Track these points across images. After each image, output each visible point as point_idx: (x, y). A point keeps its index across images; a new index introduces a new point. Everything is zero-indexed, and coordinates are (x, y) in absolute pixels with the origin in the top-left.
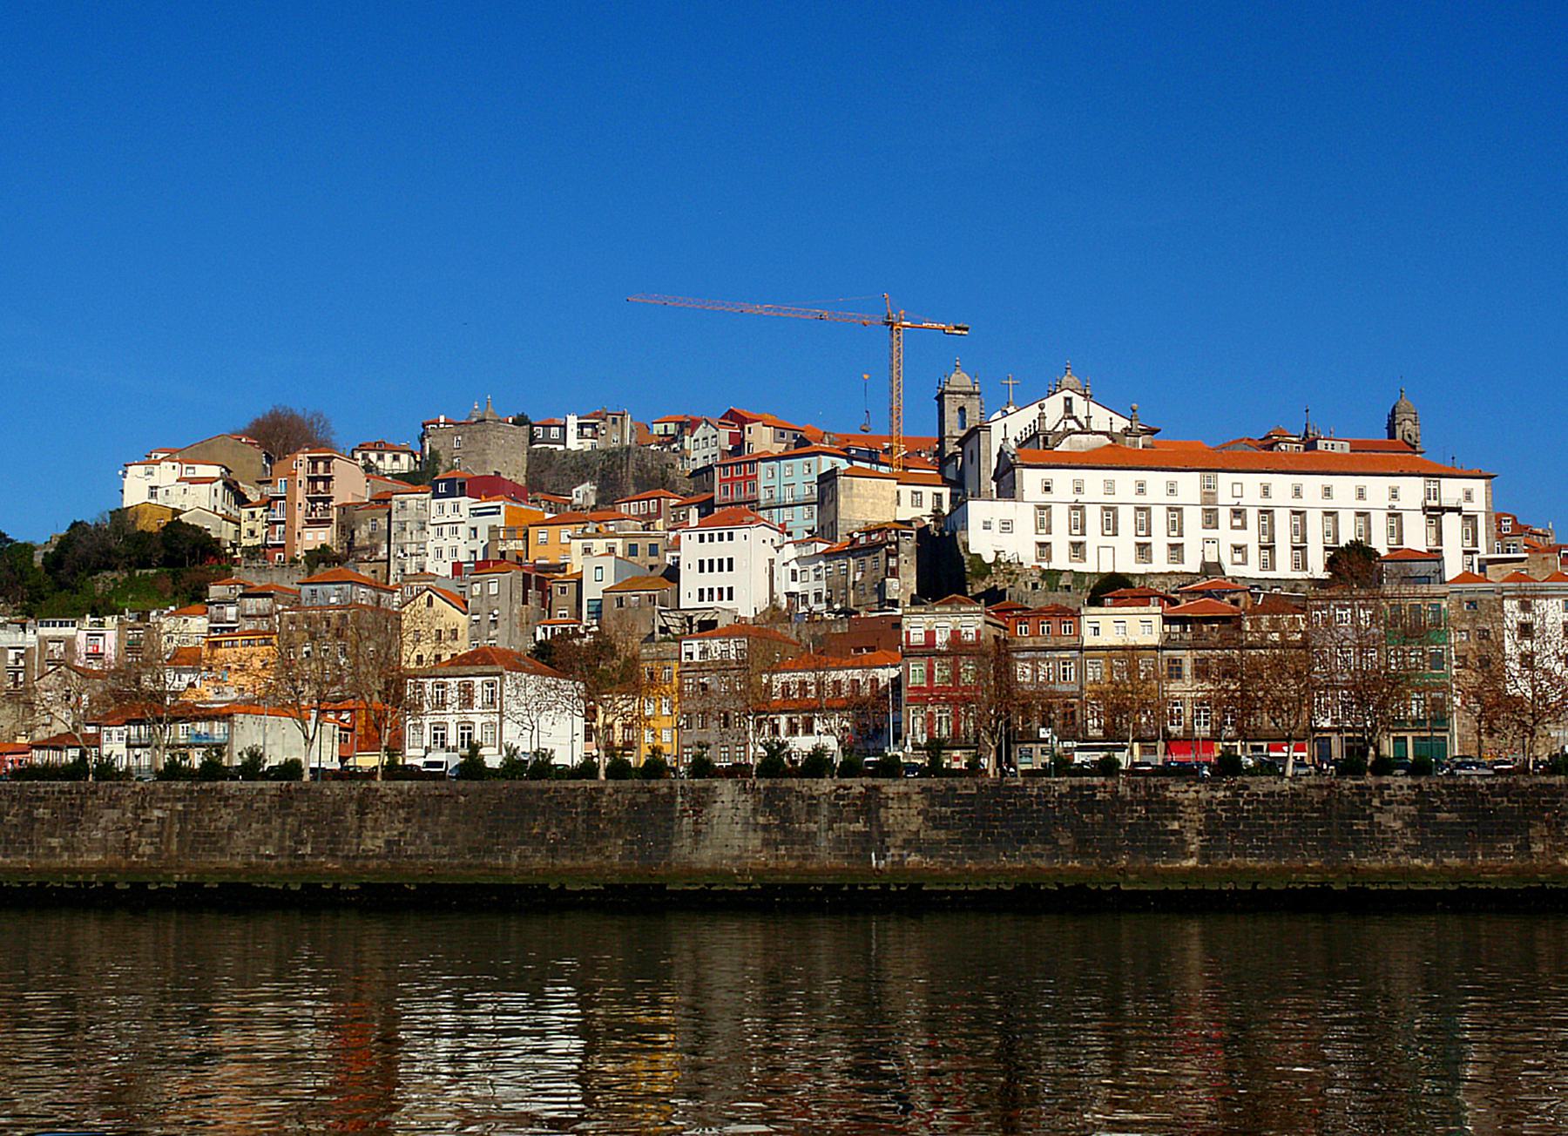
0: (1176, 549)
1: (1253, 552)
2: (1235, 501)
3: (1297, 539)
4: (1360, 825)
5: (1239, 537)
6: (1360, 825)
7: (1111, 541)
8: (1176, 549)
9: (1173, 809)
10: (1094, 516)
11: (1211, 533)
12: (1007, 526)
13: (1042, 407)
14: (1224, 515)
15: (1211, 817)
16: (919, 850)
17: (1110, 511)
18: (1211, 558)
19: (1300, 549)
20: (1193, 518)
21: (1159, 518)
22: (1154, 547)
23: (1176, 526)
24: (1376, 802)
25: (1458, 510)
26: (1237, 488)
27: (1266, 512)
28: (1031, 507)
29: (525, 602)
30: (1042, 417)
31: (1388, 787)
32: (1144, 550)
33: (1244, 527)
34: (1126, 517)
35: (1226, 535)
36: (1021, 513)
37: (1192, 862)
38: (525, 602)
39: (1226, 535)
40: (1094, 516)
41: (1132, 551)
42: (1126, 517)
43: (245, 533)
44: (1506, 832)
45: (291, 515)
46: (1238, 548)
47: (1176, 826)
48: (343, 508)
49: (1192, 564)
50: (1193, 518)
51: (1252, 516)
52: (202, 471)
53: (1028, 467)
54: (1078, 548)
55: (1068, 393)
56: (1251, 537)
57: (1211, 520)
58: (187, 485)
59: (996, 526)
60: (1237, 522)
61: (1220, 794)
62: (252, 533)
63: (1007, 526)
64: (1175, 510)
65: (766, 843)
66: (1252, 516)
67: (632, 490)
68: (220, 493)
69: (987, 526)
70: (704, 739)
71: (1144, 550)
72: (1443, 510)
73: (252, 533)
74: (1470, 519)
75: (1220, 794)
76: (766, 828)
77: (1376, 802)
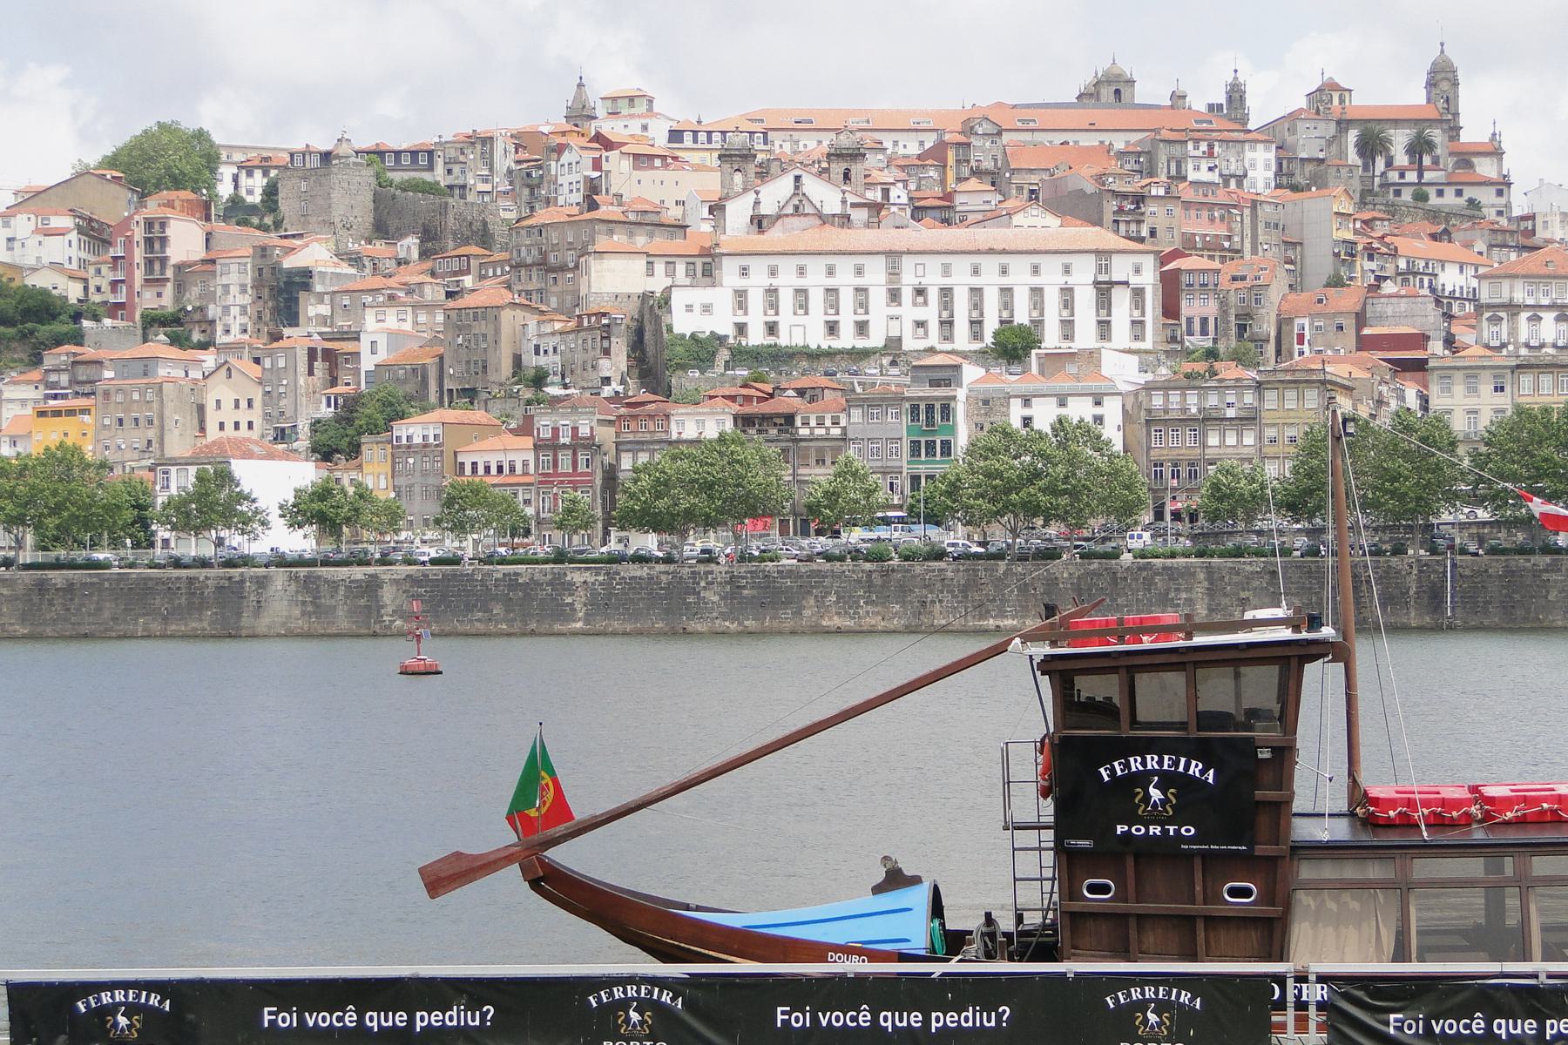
0: (862, 328)
1: (934, 327)
2: (916, 282)
3: (975, 314)
4: (691, 599)
5: (921, 314)
6: (691, 599)
7: (801, 319)
8: (862, 328)
9: (570, 588)
10: (786, 300)
11: (895, 311)
12: (707, 309)
13: (757, 193)
14: (907, 294)
15: (595, 595)
16: (401, 617)
17: (802, 293)
18: (895, 333)
19: (976, 325)
20: (878, 297)
21: (847, 299)
22: (841, 325)
23: (863, 303)
24: (703, 584)
25: (1126, 283)
26: (920, 272)
27: (946, 292)
28: (730, 292)
29: (311, 372)
30: (757, 203)
31: (711, 572)
32: (832, 328)
33: (926, 303)
34: (817, 299)
35: (909, 311)
36: (721, 297)
37: (579, 625)
38: (311, 372)
39: (909, 311)
40: (786, 300)
41: (822, 329)
42: (817, 299)
43: (92, 289)
44: (786, 604)
45: (130, 274)
46: (920, 324)
47: (569, 600)
48: (179, 268)
49: (876, 340)
50: (878, 297)
51: (933, 295)
52: (57, 222)
53: (1158, 107)
54: (772, 328)
55: (797, 172)
56: (931, 313)
57: (894, 296)
58: (41, 238)
59: (697, 309)
60: (920, 299)
61: (601, 578)
62: (98, 289)
63: (707, 309)
64: (861, 291)
65: (303, 613)
66: (933, 295)
67: (451, 244)
68: (75, 243)
69: (689, 308)
70: (1007, 379)
71: (832, 328)
72: (1112, 284)
73: (98, 289)
74: (1138, 293)
75: (601, 578)
76: (304, 603)
77: (703, 584)
